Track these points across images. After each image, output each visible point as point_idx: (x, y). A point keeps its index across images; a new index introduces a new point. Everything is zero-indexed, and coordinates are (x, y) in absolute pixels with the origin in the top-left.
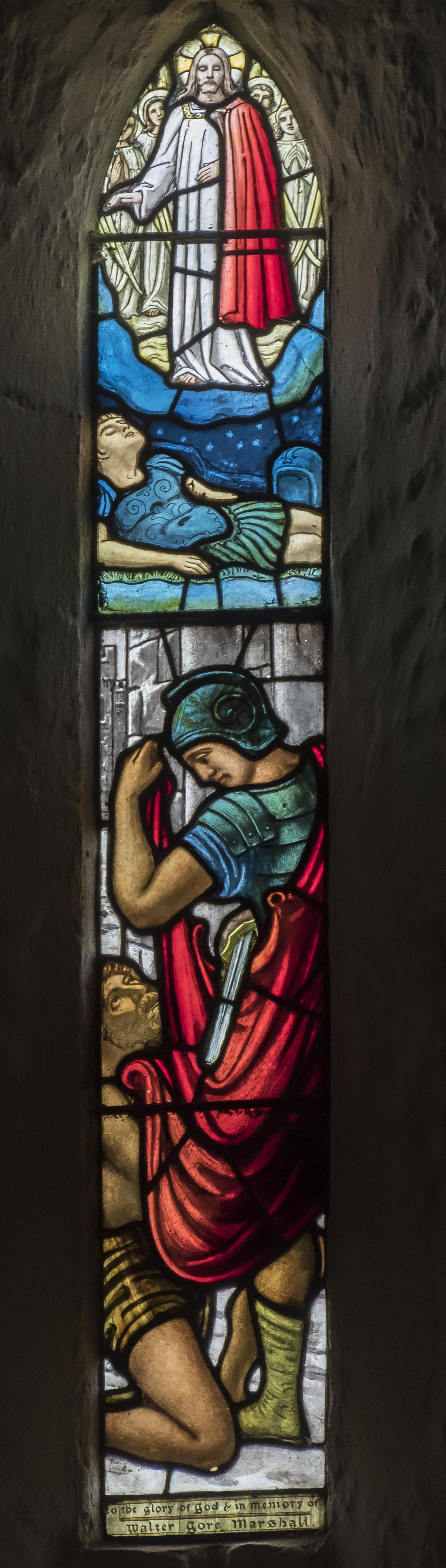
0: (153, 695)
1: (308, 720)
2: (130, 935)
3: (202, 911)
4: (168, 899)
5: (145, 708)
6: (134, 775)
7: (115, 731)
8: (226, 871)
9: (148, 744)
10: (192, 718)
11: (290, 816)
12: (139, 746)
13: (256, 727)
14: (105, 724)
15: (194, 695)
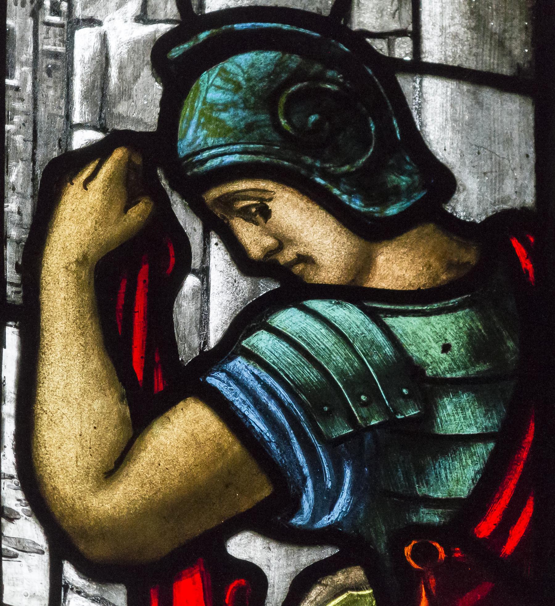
0: (134, 47)
1: (501, 176)
2: (70, 573)
3: (245, 547)
4: (170, 508)
5: (113, 72)
6: (83, 217)
7: (42, 109)
8: (306, 471)
9: (118, 154)
10: (224, 116)
11: (460, 374)
12: (97, 153)
13: (377, 167)
14: (17, 89)
15: (229, 65)
